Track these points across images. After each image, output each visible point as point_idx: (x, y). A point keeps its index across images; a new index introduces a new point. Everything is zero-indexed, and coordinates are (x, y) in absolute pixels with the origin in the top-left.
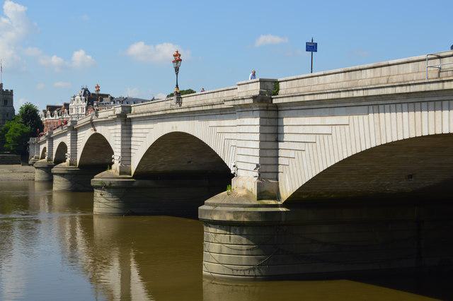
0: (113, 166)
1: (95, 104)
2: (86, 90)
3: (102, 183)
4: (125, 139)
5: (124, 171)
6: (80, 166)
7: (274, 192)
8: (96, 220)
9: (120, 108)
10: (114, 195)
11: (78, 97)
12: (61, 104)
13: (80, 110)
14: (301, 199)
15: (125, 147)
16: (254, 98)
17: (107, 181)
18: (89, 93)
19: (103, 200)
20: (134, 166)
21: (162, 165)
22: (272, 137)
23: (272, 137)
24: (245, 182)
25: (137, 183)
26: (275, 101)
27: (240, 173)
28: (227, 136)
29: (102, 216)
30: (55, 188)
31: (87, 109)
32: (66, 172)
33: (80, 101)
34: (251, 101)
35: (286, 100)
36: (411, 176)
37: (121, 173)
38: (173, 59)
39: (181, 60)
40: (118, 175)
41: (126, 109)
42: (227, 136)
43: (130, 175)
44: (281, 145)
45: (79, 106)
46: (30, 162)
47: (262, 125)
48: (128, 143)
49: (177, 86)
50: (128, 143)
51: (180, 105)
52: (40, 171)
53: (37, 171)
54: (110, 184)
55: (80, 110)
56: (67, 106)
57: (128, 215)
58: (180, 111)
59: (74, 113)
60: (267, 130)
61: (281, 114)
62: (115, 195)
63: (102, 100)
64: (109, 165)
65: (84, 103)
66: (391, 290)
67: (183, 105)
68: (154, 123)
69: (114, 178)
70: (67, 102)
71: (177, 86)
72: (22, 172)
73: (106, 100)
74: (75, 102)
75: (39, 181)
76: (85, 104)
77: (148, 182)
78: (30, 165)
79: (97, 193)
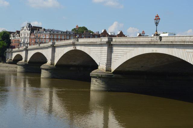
0: (47, 62)
1: (35, 32)
2: (30, 24)
3: (97, 75)
4: (109, 54)
5: (26, 61)
6: (29, 62)
7: (110, 70)
8: (92, 94)
9: (108, 39)
10: (103, 81)
11: (25, 28)
12: (15, 31)
13: (26, 35)
14: (116, 72)
15: (109, 58)
16: (106, 42)
17: (100, 74)
18: (31, 26)
19: (97, 83)
20: (56, 62)
21: (64, 63)
22: (54, 51)
23: (54, 51)
24: (49, 62)
25: (114, 76)
26: (112, 43)
27: (100, 65)
28: (94, 51)
29: (95, 91)
30: (42, 76)
31: (30, 35)
32: (49, 68)
33: (27, 30)
34: (106, 43)
35: (114, 43)
36: (142, 67)
37: (106, 71)
38: (155, 18)
39: (160, 19)
40: (105, 71)
41: (110, 39)
42: (94, 51)
43: (111, 71)
44: (55, 53)
45: (26, 33)
46: (7, 62)
47: (108, 49)
48: (110, 56)
49: (156, 31)
50: (110, 56)
51: (161, 41)
52: (21, 67)
53: (18, 66)
54: (102, 76)
55: (26, 35)
56: (18, 32)
57: (109, 91)
58: (160, 43)
59: (23, 36)
60: (109, 50)
61: (113, 46)
62: (104, 81)
63: (39, 30)
64: (21, 59)
65: (29, 31)
66: (170, 99)
67: (162, 40)
68: (134, 47)
69: (101, 73)
70: (19, 30)
71: (156, 31)
72: (4, 67)
73: (41, 30)
74: (23, 31)
75: (20, 72)
76: (29, 32)
77: (120, 76)
78: (7, 63)
79: (93, 80)
